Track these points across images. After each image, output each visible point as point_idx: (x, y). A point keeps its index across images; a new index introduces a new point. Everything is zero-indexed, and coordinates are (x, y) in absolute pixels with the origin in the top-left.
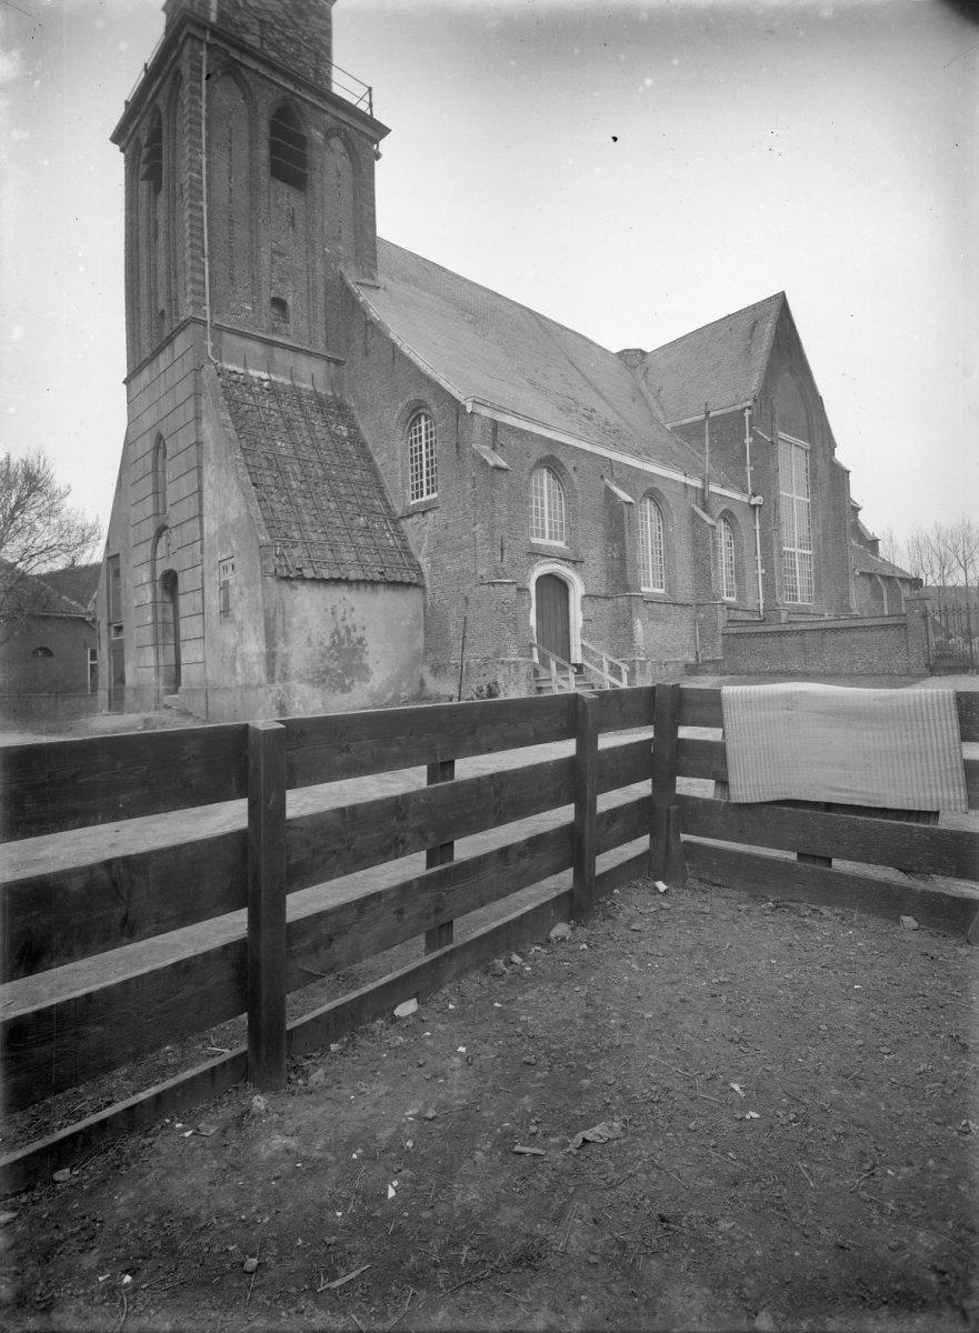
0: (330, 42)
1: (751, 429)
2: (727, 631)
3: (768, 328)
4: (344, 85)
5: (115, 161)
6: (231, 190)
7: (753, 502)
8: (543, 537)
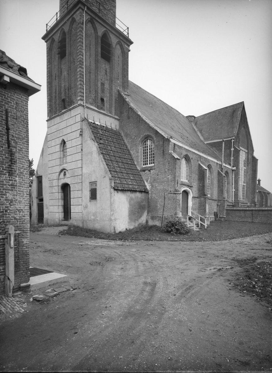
0: (115, 10)
1: (233, 146)
2: (227, 208)
3: (239, 113)
4: (119, 26)
5: (43, 45)
6: (90, 61)
7: (233, 169)
8: (183, 179)
